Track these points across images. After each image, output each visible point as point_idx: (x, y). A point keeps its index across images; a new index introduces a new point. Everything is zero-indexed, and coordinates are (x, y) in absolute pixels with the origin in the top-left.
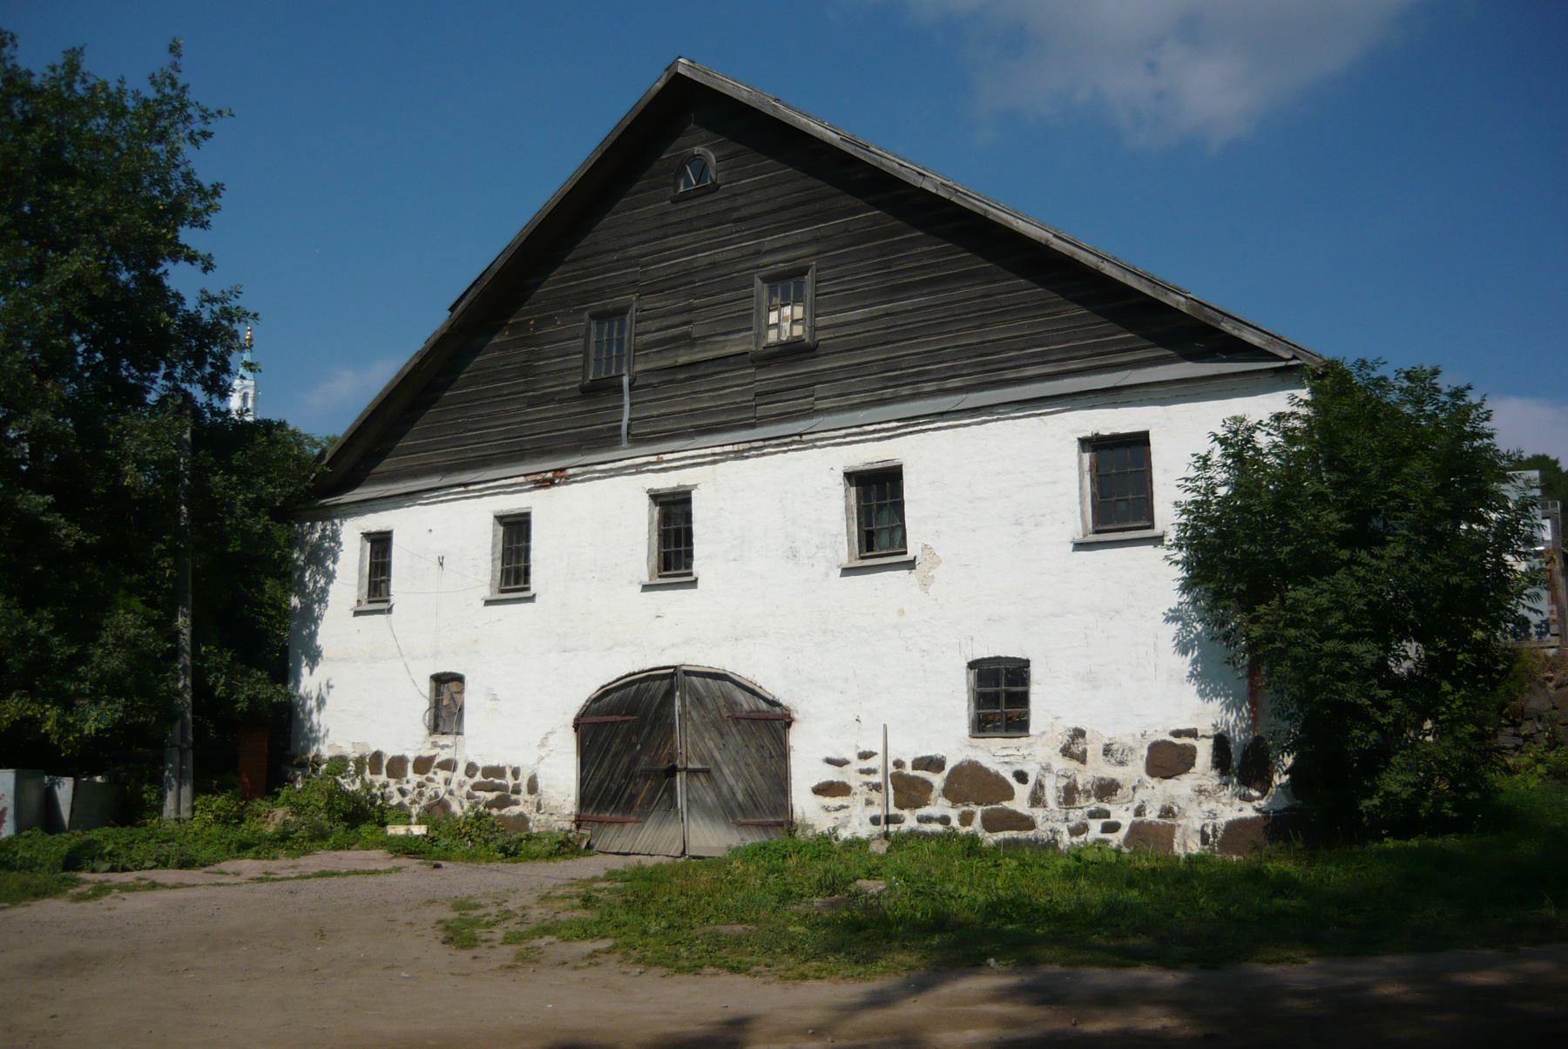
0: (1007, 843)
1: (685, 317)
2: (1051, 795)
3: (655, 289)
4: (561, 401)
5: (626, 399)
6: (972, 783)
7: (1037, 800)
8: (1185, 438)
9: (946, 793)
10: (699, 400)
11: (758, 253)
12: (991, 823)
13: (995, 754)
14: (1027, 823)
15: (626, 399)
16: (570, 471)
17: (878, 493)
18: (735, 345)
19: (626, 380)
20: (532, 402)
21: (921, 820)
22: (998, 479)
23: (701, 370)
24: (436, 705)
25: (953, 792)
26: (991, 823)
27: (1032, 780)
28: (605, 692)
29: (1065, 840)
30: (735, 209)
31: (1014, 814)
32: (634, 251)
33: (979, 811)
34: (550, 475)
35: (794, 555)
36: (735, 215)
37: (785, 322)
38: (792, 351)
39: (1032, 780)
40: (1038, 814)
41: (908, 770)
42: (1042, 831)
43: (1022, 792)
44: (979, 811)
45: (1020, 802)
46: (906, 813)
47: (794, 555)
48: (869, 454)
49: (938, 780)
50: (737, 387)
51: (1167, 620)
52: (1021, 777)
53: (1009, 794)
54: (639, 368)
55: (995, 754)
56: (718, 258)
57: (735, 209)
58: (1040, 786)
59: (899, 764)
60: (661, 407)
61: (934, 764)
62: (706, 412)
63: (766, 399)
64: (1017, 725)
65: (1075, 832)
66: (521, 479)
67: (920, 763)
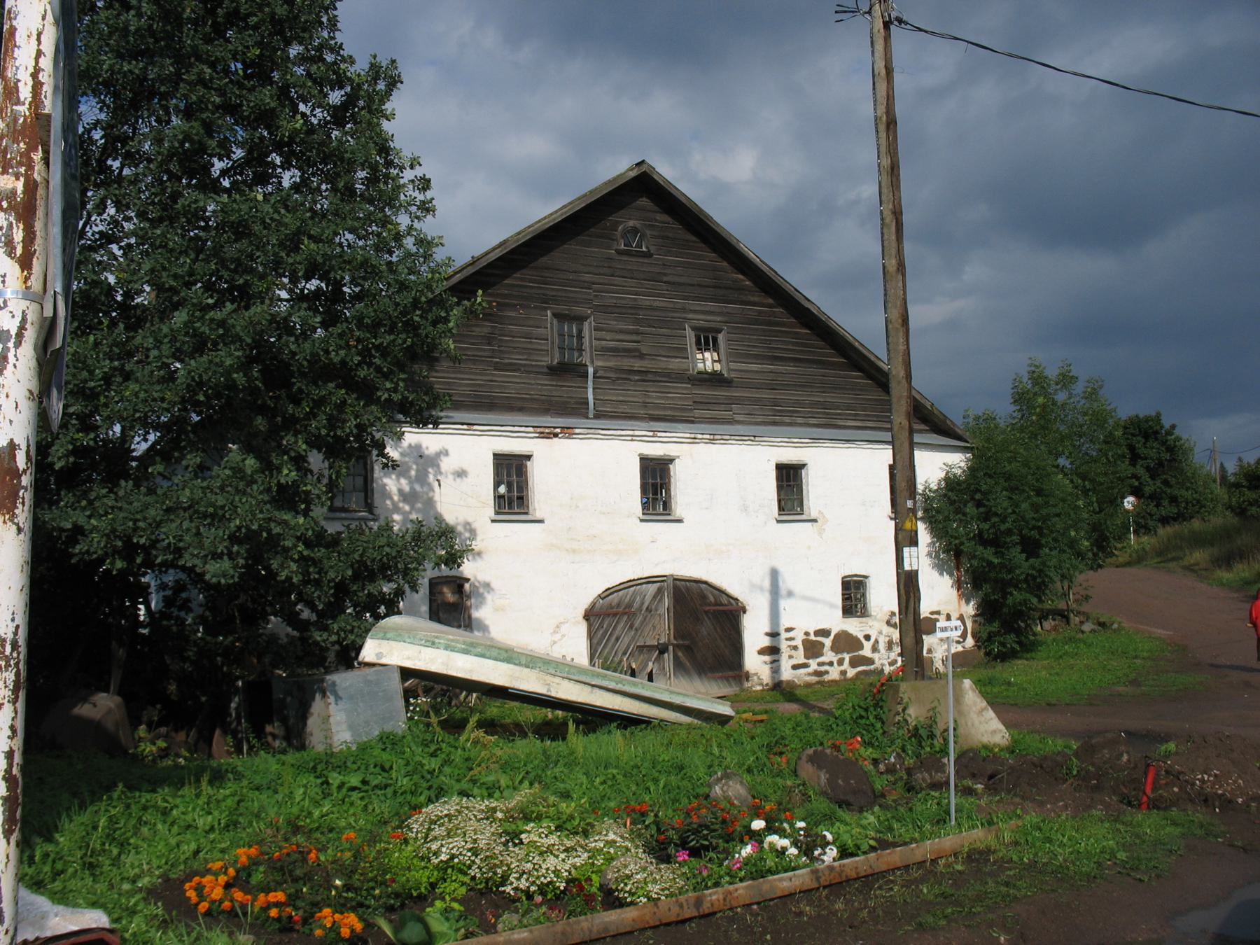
0: (860, 673)
1: (634, 337)
2: (882, 646)
3: (606, 309)
4: (528, 372)
5: (590, 383)
6: (845, 642)
7: (875, 649)
8: (934, 466)
9: (833, 648)
10: (649, 397)
11: (684, 310)
12: (853, 663)
13: (854, 627)
14: (870, 661)
15: (590, 383)
16: (577, 431)
17: (789, 478)
18: (675, 364)
19: (591, 370)
20: (498, 367)
21: (819, 664)
22: (850, 474)
23: (650, 377)
24: (846, 598)
25: (836, 648)
26: (853, 663)
27: (873, 639)
28: (609, 592)
29: (887, 669)
30: (665, 275)
31: (864, 657)
32: (587, 277)
33: (847, 657)
34: (558, 430)
35: (745, 509)
36: (665, 279)
37: (707, 361)
38: (714, 379)
39: (873, 639)
40: (876, 656)
41: (812, 637)
42: (877, 665)
43: (867, 646)
44: (847, 657)
45: (867, 651)
46: (811, 661)
47: (745, 509)
48: (789, 454)
49: (828, 642)
50: (679, 394)
51: (479, 554)
52: (867, 637)
53: (861, 647)
54: (600, 363)
55: (854, 627)
56: (657, 303)
57: (665, 275)
58: (877, 641)
59: (807, 634)
60: (618, 395)
61: (824, 633)
62: (657, 406)
63: (714, 406)
64: (864, 613)
65: (891, 664)
66: (531, 429)
67: (818, 633)
